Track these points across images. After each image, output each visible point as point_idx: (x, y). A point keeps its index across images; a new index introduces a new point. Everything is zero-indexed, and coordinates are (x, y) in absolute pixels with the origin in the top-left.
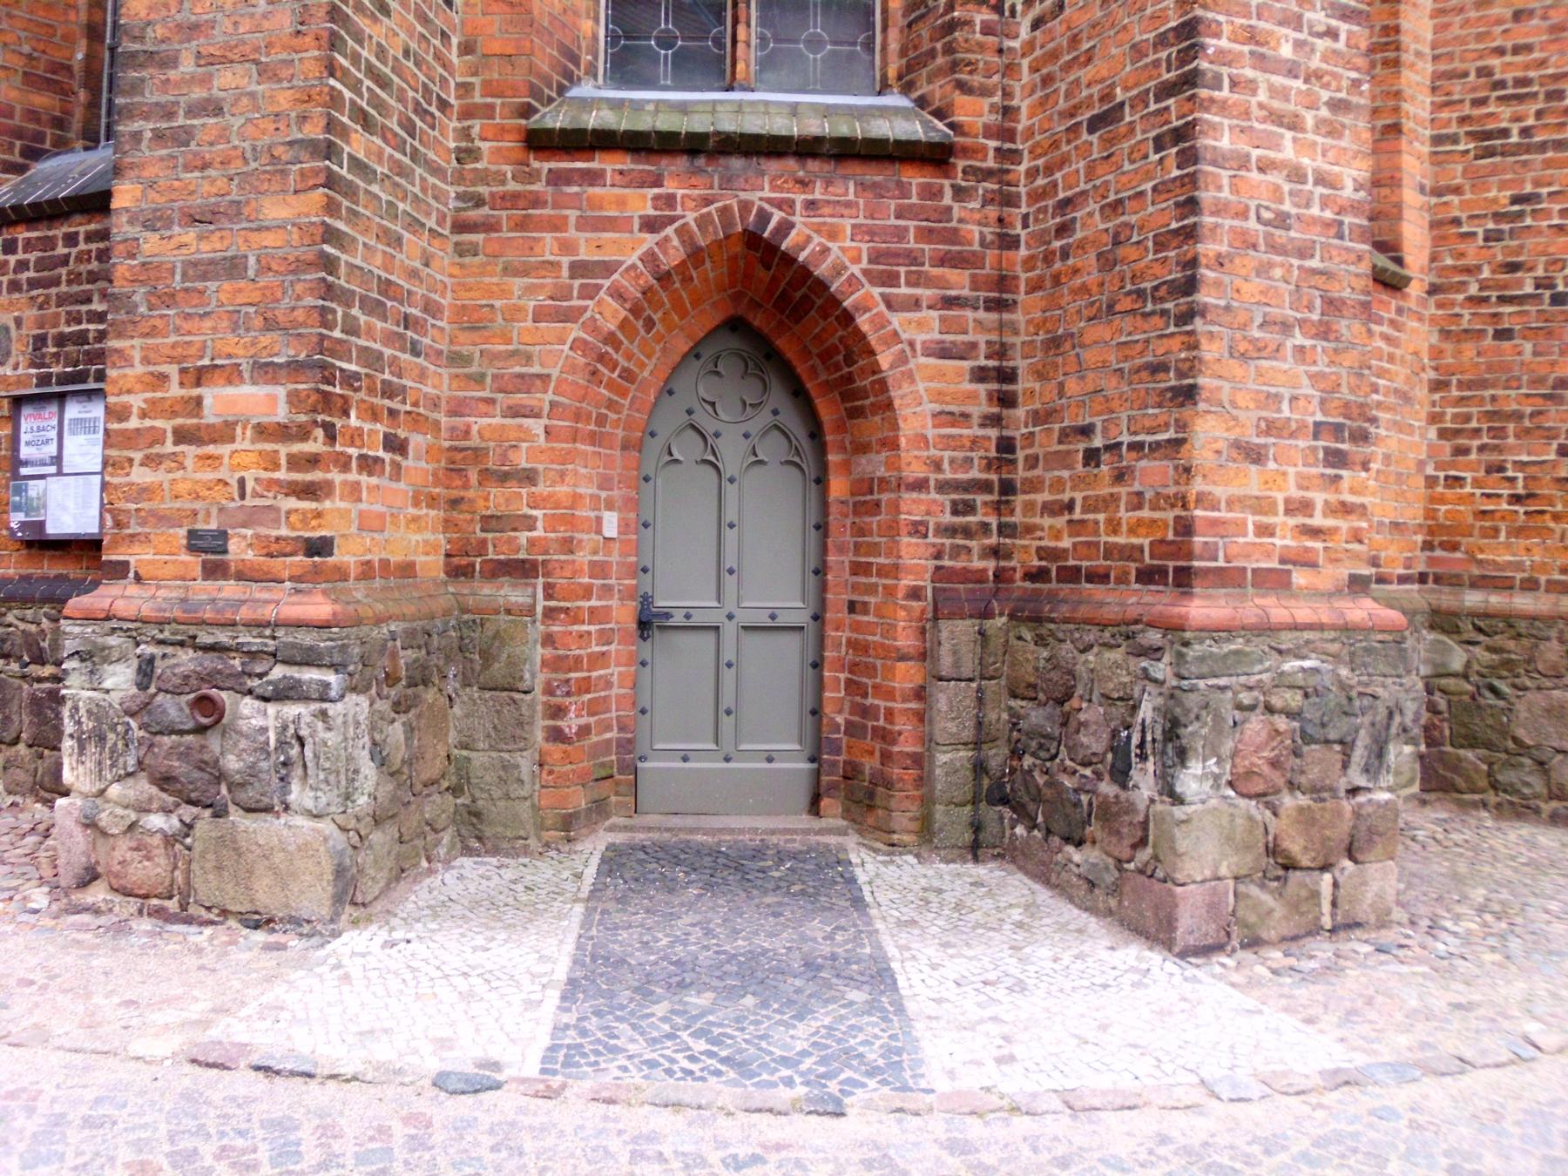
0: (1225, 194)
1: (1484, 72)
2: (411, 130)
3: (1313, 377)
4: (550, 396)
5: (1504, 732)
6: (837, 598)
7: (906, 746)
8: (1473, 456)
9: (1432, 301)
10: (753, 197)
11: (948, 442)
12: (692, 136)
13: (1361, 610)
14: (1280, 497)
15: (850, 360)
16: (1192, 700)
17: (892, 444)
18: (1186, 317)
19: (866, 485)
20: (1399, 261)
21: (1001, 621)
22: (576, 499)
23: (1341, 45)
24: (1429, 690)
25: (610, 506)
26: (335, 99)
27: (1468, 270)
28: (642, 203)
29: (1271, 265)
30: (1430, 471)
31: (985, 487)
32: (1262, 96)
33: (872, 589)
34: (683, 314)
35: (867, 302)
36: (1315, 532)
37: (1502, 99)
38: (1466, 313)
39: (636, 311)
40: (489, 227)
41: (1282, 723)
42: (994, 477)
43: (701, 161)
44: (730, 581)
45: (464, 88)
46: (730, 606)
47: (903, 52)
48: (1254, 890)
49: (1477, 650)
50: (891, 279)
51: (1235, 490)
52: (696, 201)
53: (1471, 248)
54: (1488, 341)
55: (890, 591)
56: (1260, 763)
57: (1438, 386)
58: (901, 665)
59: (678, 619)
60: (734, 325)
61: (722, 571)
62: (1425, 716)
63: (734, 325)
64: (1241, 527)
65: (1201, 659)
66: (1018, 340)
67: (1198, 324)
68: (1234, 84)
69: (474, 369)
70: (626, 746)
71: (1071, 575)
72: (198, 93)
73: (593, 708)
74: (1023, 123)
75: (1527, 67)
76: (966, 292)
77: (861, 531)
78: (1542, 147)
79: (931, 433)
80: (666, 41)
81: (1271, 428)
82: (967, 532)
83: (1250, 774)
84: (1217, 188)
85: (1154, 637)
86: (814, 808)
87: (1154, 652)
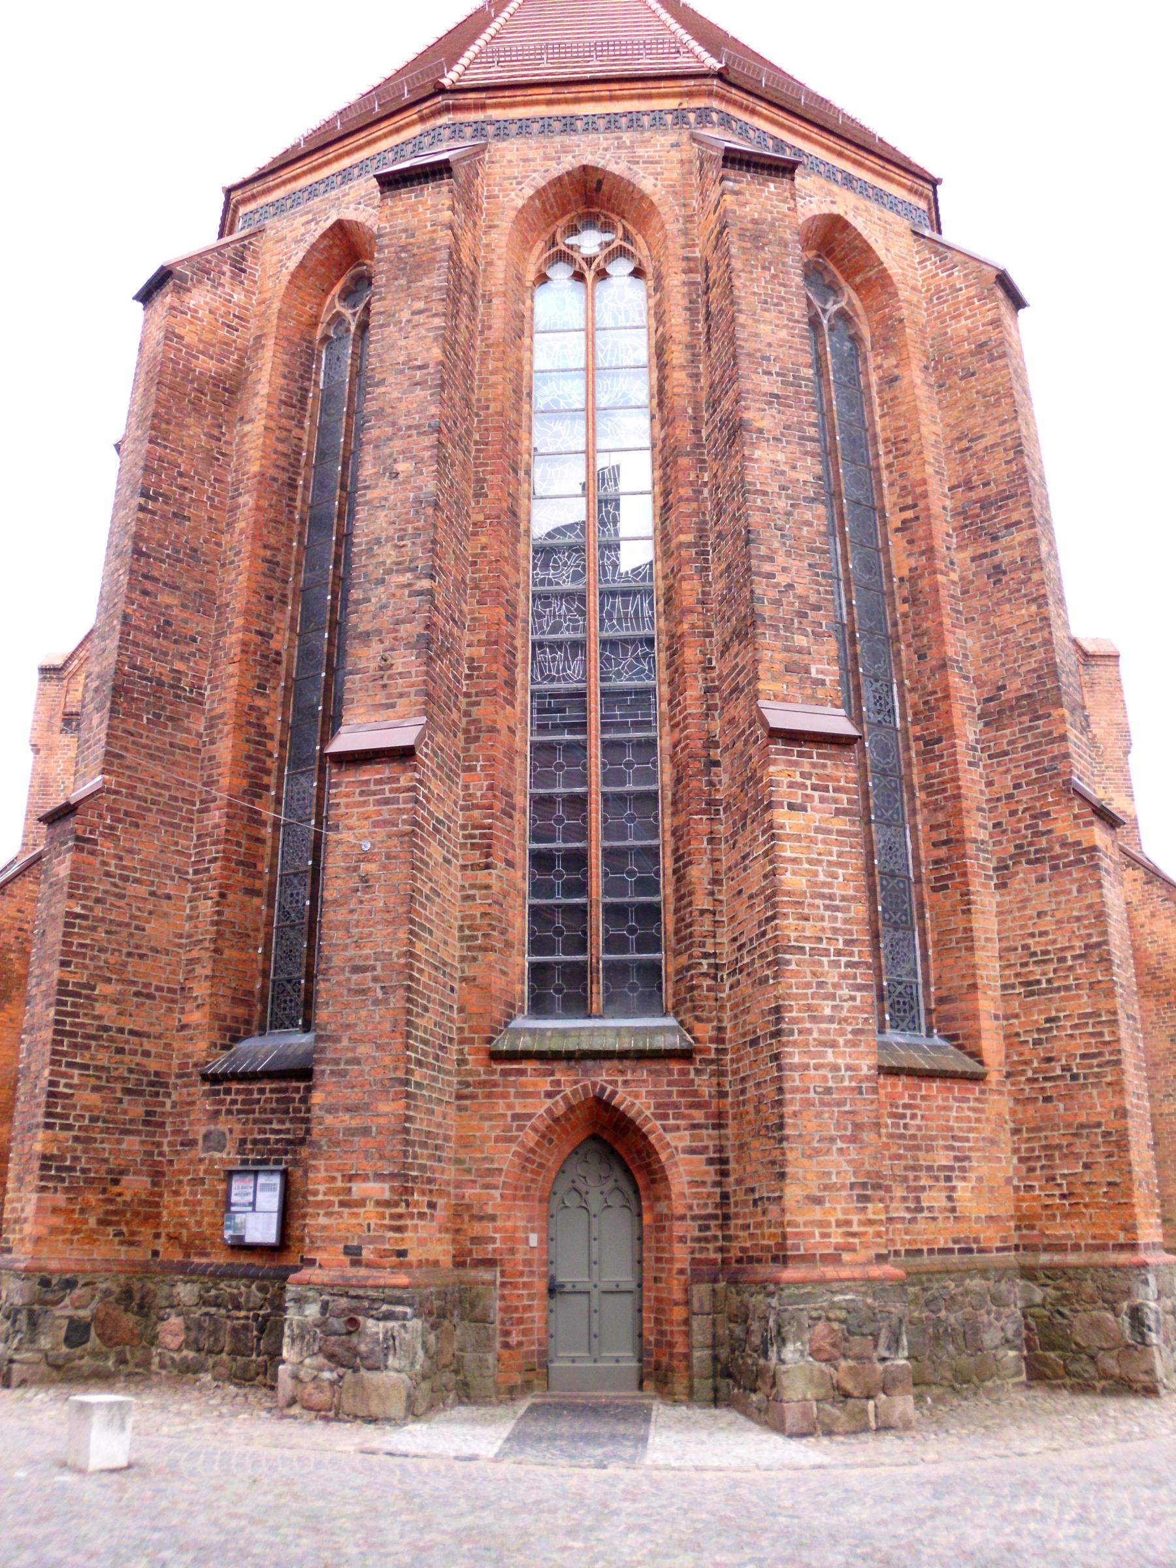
0: (797, 1083)
1: (1026, 947)
2: (437, 1058)
3: (849, 1162)
4: (502, 1179)
5: (1068, 1339)
6: (649, 1275)
7: (680, 1349)
8: (1038, 1172)
9: (1008, 1083)
10: (598, 1079)
11: (696, 1196)
12: (568, 1052)
13: (888, 1269)
14: (833, 1220)
15: (649, 1156)
16: (786, 1315)
17: (668, 1197)
18: (781, 1141)
19: (660, 1217)
20: (981, 1063)
21: (723, 1284)
22: (515, 1229)
23: (858, 1003)
24: (1025, 1317)
25: (533, 1230)
26: (409, 1058)
27: (1026, 1063)
28: (545, 1084)
29: (822, 1112)
30: (1015, 1182)
31: (715, 1217)
32: (815, 1035)
33: (662, 1270)
34: (567, 1133)
35: (653, 1128)
36: (854, 1235)
37: (1035, 963)
38: (1027, 1088)
39: (543, 1136)
40: (473, 1097)
41: (836, 1326)
42: (719, 1212)
43: (573, 1063)
44: (595, 1268)
45: (461, 1030)
46: (595, 1280)
47: (674, 995)
48: (828, 1407)
49: (1049, 1290)
50: (665, 1117)
51: (808, 1217)
52: (570, 1083)
53: (1026, 1049)
54: (1040, 1103)
55: (670, 1270)
56: (825, 1344)
57: (1016, 1131)
58: (676, 1309)
59: (568, 1288)
60: (594, 1137)
61: (591, 1263)
62: (1024, 1333)
63: (594, 1137)
64: (812, 1235)
65: (790, 1296)
66: (729, 1143)
67: (785, 1144)
68: (800, 1032)
69: (466, 1166)
70: (543, 1353)
71: (751, 1260)
72: (350, 1055)
73: (525, 1332)
74: (728, 1035)
75: (1047, 944)
76: (702, 1121)
77: (658, 1241)
78: (1058, 989)
79: (687, 1191)
80: (558, 990)
81: (826, 1187)
82: (706, 1240)
83: (819, 1350)
84: (794, 1080)
85: (771, 1288)
86: (640, 1387)
87: (771, 1294)
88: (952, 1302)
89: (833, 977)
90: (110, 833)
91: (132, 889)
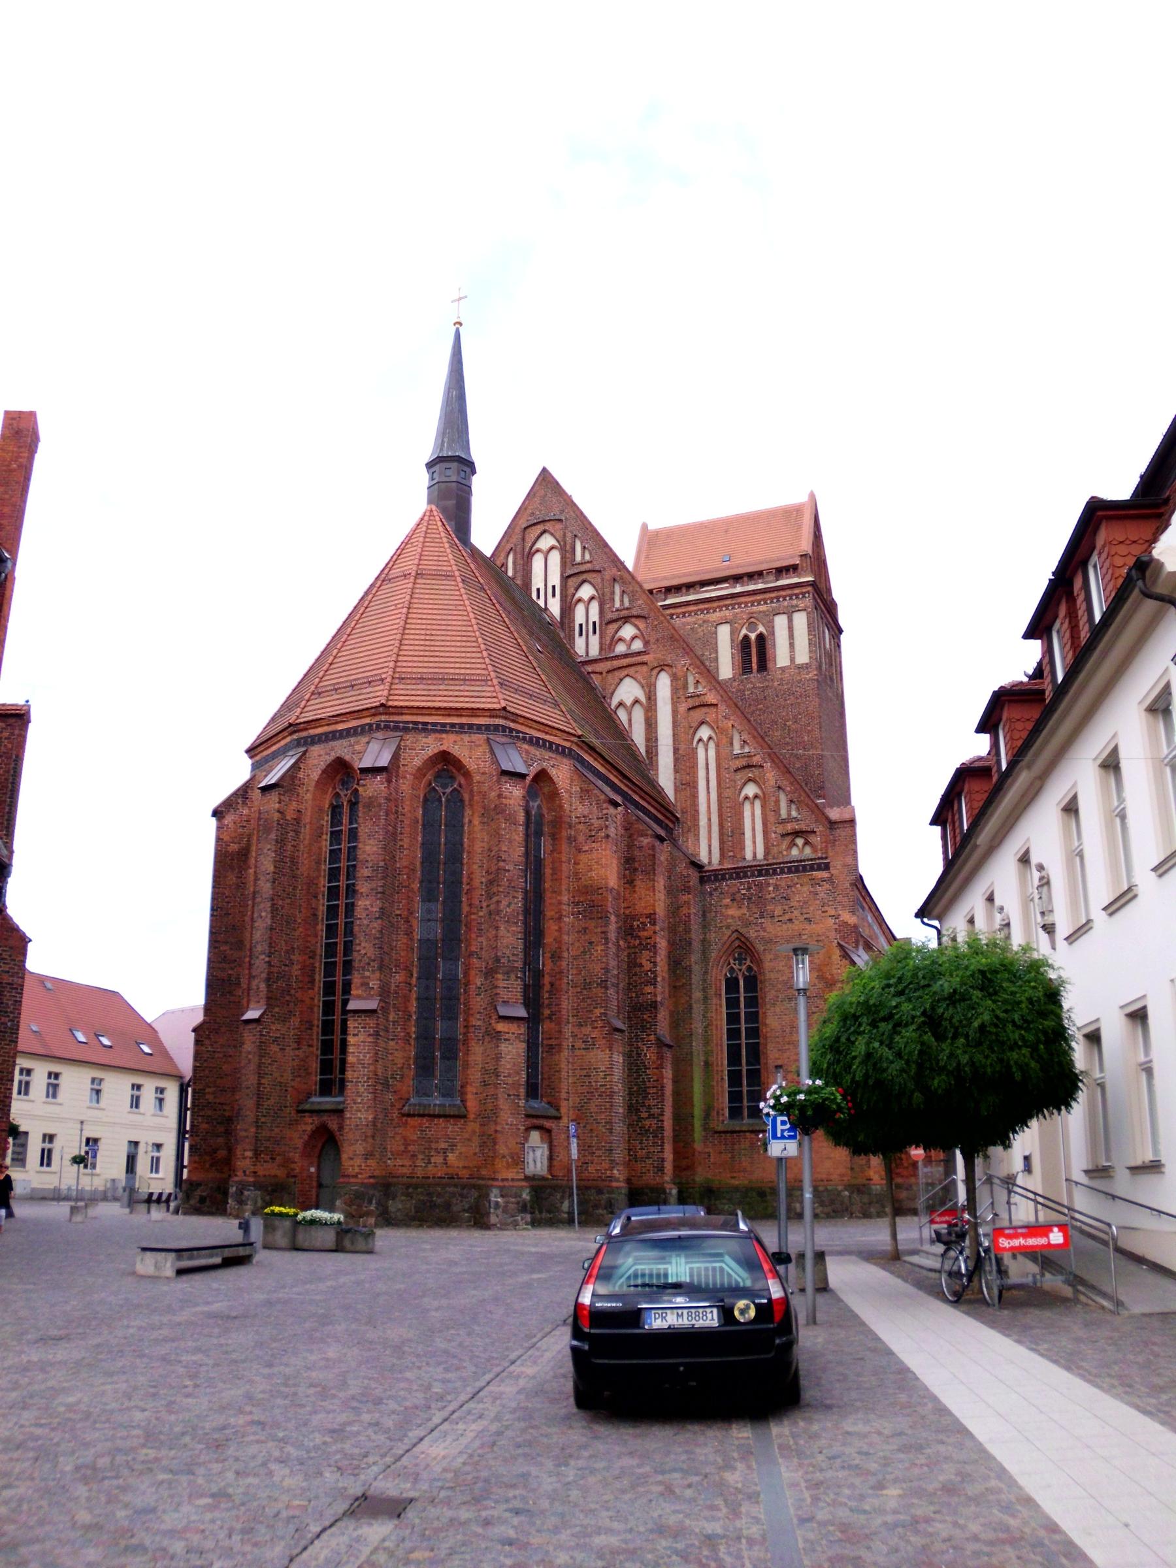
13: (372, 1180)
28: (310, 1121)
88: (439, 1195)
89: (362, 1090)
90: (208, 1037)
91: (217, 1055)
